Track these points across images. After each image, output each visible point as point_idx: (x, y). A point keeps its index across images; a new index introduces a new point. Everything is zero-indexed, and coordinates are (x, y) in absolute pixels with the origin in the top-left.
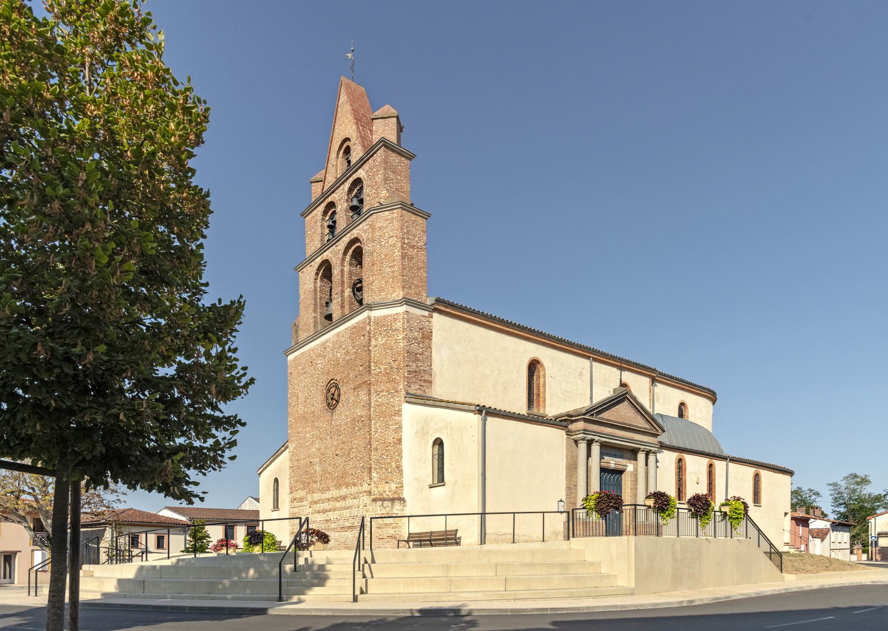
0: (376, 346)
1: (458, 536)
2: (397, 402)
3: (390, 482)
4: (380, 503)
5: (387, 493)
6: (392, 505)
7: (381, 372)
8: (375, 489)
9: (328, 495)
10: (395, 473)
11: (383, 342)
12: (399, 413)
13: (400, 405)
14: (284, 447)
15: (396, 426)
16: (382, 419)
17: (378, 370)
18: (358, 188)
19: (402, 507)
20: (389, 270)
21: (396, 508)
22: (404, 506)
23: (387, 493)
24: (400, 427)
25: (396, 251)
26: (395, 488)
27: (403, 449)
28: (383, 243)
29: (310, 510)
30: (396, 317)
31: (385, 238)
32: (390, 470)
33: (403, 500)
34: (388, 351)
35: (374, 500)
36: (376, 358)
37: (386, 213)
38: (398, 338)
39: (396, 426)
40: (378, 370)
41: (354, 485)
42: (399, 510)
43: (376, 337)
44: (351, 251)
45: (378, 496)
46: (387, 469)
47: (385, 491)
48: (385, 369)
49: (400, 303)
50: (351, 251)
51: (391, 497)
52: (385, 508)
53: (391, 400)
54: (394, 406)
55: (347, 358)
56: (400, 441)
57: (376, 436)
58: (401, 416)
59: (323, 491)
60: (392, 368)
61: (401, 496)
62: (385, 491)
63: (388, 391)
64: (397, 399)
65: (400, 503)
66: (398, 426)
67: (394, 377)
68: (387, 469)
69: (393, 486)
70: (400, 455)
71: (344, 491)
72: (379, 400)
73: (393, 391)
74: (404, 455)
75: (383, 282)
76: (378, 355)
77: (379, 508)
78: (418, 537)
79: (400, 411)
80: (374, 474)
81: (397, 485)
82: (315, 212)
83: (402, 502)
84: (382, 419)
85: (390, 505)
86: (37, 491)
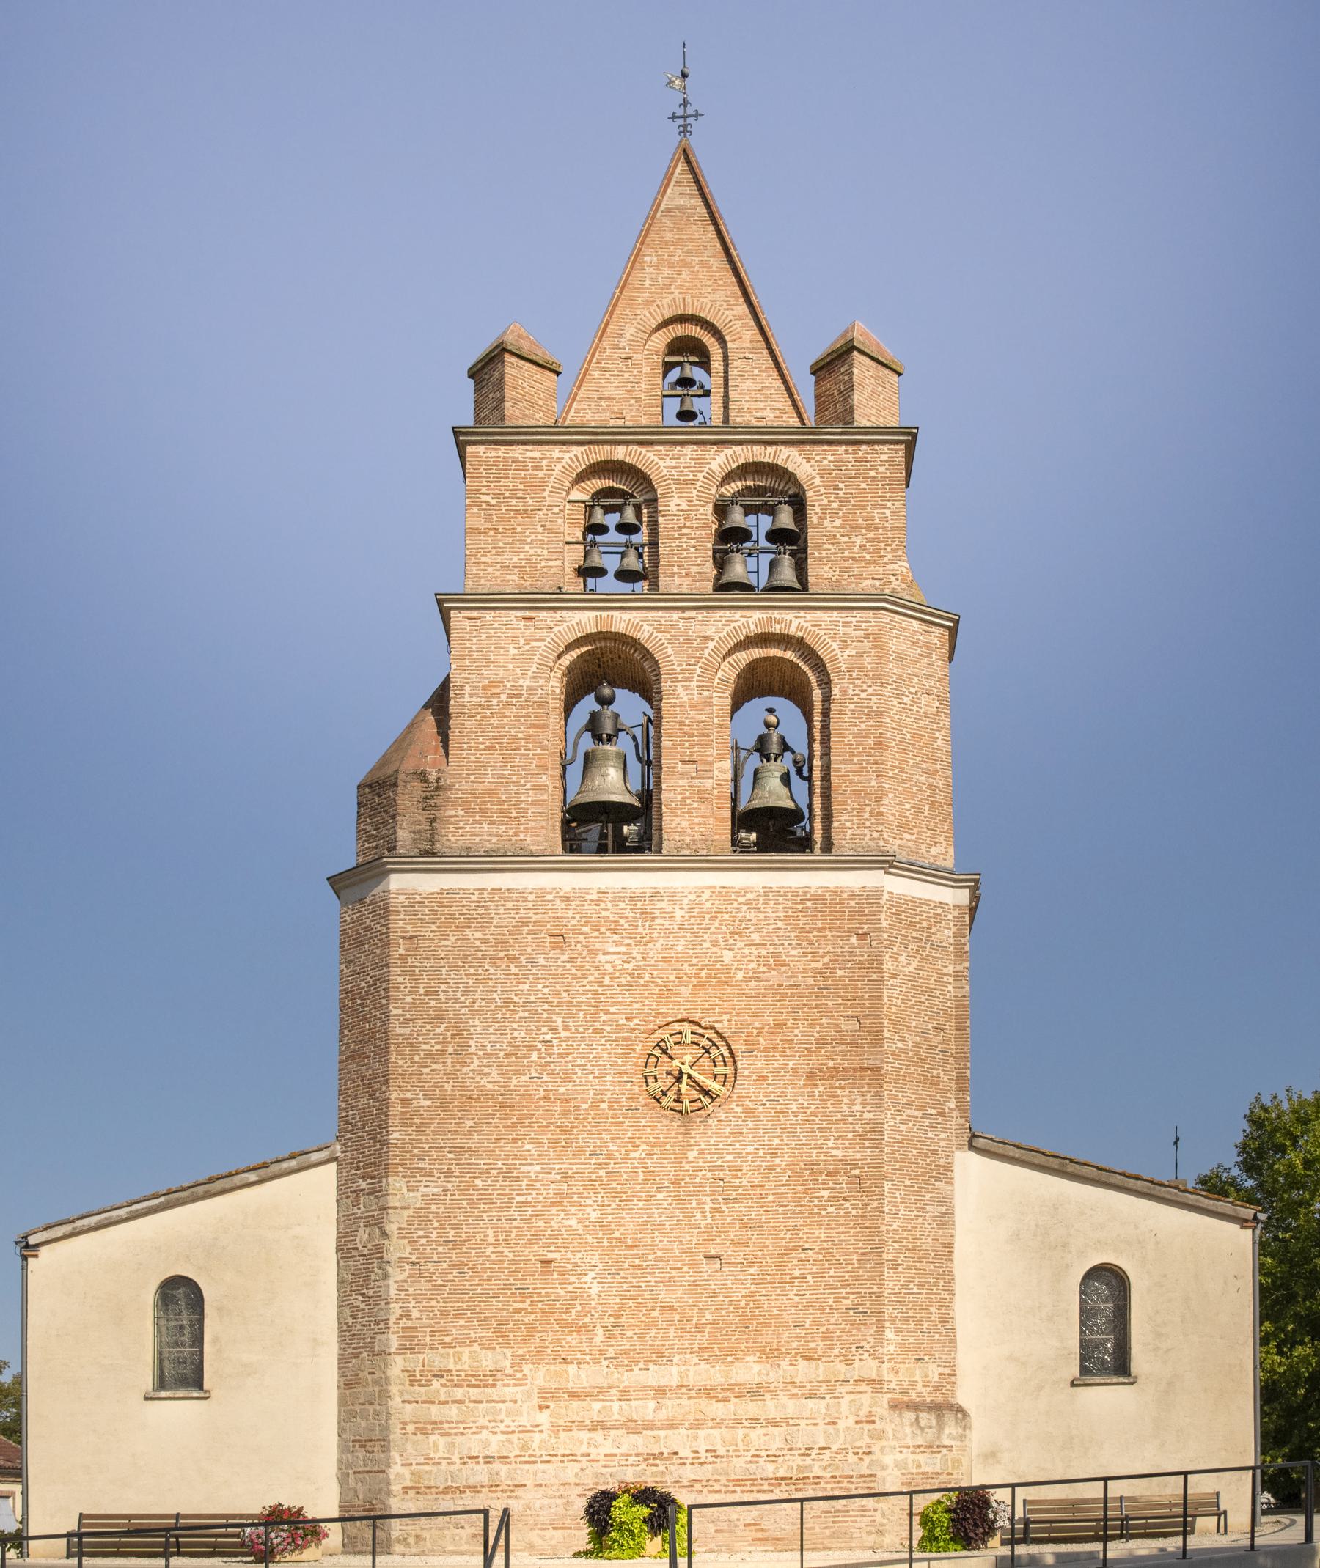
0: (894, 976)
1: (1222, 1508)
2: (942, 1144)
3: (927, 1357)
4: (910, 1416)
5: (920, 1388)
6: (940, 1426)
7: (905, 1051)
8: (891, 1377)
9: (669, 1375)
10: (937, 1336)
11: (911, 969)
12: (945, 1172)
13: (950, 1154)
14: (263, 1172)
15: (939, 1209)
16: (908, 1182)
17: (900, 1045)
18: (750, 483)
19: (960, 1430)
20: (923, 779)
21: (947, 1431)
22: (964, 1428)
23: (920, 1388)
24: (950, 1213)
25: (937, 734)
26: (936, 1378)
27: (957, 1272)
28: (906, 700)
29: (543, 1418)
30: (939, 911)
31: (913, 690)
32: (925, 1325)
33: (959, 1410)
34: (923, 999)
35: (895, 1406)
36: (894, 1009)
37: (915, 623)
38: (945, 971)
39: (939, 1209)
40: (900, 1045)
41: (807, 1358)
42: (954, 1439)
43: (895, 950)
44: (757, 653)
45: (898, 1396)
46: (919, 1323)
47: (914, 1384)
48: (917, 1046)
49: (954, 880)
50: (757, 653)
51: (928, 1400)
52: (922, 1429)
53: (930, 1135)
54: (934, 1153)
55: (774, 976)
56: (947, 1250)
57: (895, 1226)
58: (950, 1181)
59: (625, 1360)
60: (930, 1047)
61: (953, 1401)
62: (914, 1384)
63: (921, 1108)
64: (943, 1136)
65: (957, 1418)
66: (944, 1209)
67: (935, 1073)
68: (919, 1323)
69: (934, 1371)
70: (949, 1283)
71: (750, 1370)
72: (903, 1127)
73: (934, 1112)
74: (958, 1287)
75: (908, 806)
76: (899, 1002)
77: (908, 1430)
78: (1066, 1511)
79: (948, 1168)
80: (889, 1334)
81: (941, 1370)
82: (555, 452)
83: (960, 1415)
84: (908, 1182)
85: (934, 1422)
86: (944, 1357)
